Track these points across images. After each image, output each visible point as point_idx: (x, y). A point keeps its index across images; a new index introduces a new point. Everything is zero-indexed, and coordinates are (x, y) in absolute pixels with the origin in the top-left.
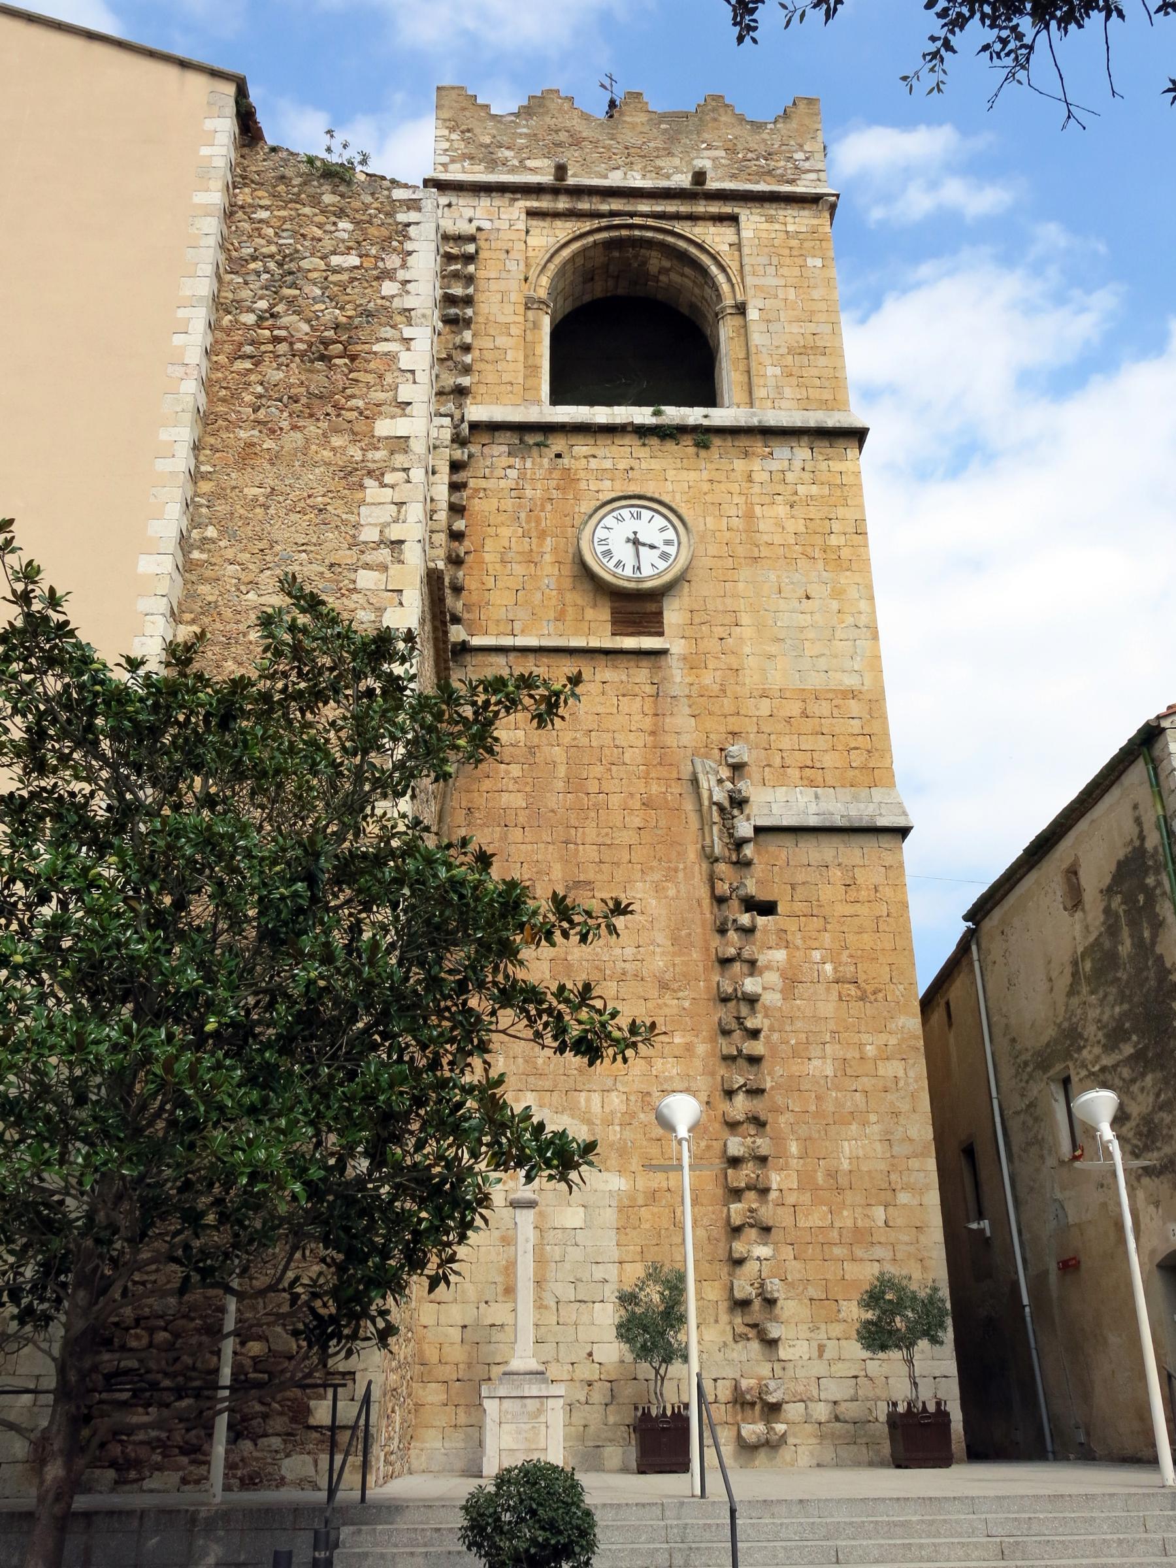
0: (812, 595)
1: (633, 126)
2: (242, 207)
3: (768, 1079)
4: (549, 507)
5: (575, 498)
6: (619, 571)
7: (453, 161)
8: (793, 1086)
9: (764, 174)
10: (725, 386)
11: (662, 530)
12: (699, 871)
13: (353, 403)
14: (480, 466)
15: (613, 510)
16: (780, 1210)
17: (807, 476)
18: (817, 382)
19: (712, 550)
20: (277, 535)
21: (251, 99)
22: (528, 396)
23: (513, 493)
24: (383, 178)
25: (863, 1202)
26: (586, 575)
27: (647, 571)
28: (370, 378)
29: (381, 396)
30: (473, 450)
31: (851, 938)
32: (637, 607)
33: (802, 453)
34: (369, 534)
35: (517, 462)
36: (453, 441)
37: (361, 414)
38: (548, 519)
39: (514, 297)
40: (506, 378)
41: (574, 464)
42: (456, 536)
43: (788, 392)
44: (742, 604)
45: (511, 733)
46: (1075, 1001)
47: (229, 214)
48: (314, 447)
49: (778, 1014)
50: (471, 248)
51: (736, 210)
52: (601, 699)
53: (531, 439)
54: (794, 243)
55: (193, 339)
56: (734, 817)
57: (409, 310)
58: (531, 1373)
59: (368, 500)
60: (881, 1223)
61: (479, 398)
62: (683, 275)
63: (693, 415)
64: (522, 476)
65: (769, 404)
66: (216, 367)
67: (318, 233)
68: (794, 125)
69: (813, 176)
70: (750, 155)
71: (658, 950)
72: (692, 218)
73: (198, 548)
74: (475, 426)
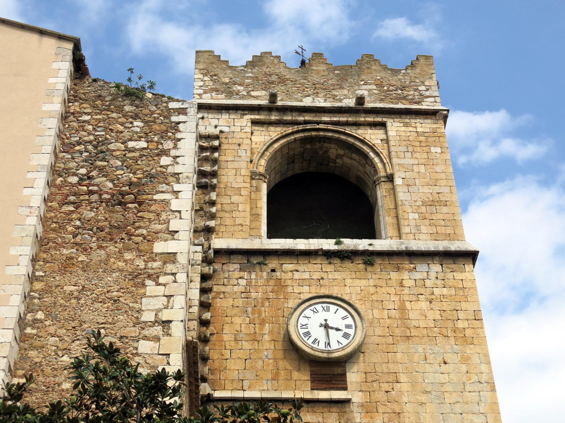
0: (448, 361)
1: (318, 72)
2: (73, 113)
4: (267, 304)
9: (401, 98)
10: (382, 223)
11: (344, 318)
14: (221, 277)
15: (311, 305)
17: (439, 282)
18: (443, 223)
19: (378, 331)
20: (85, 317)
21: (82, 52)
22: (253, 233)
24: (163, 96)
26: (292, 349)
27: (334, 346)
28: (151, 216)
29: (159, 227)
30: (216, 267)
32: (328, 370)
33: (436, 268)
34: (148, 317)
35: (246, 275)
36: (203, 261)
38: (266, 312)
39: (243, 172)
40: (238, 221)
41: (284, 276)
42: (204, 323)
43: (423, 229)
47: (64, 118)
48: (112, 260)
50: (216, 143)
51: (384, 120)
53: (254, 260)
54: (422, 138)
59: (148, 294)
61: (220, 234)
62: (351, 158)
63: (362, 244)
64: (249, 284)
65: (412, 236)
66: (50, 209)
67: (121, 128)
68: (418, 70)
69: (432, 99)
70: (391, 88)
72: (357, 125)
73: (31, 326)
74: (218, 252)
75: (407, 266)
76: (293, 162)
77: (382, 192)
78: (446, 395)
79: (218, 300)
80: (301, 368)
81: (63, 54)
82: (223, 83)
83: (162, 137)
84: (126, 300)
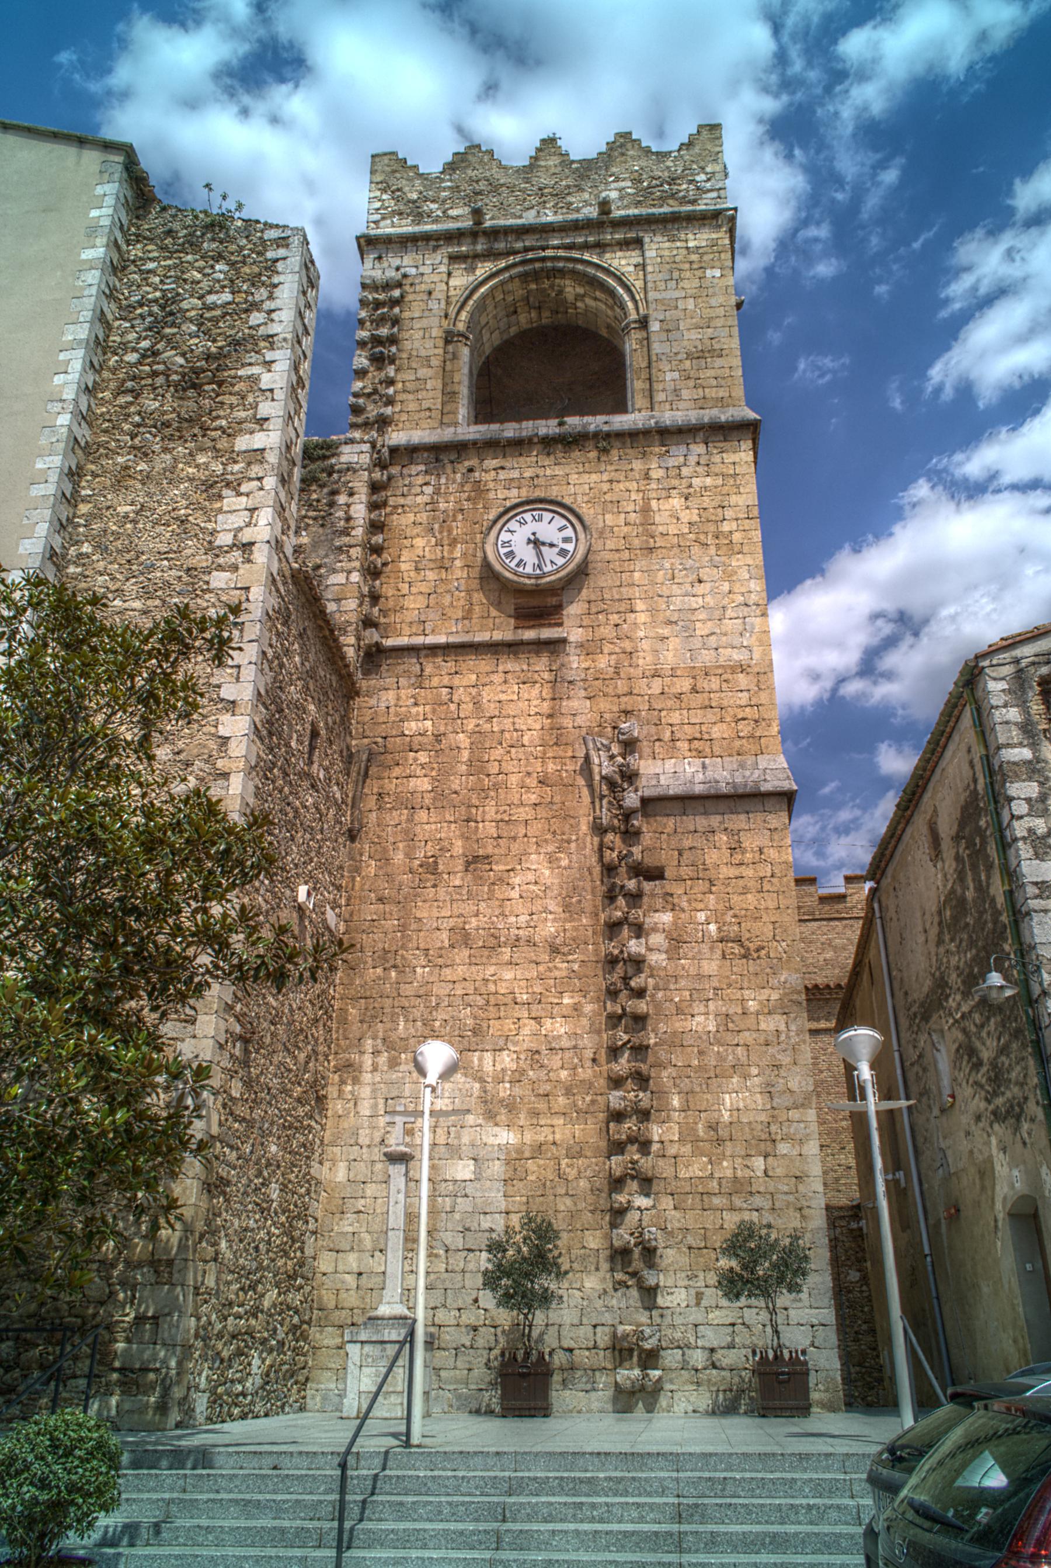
0: (705, 578)
2: (134, 261)
3: (652, 1035)
4: (460, 517)
5: (484, 507)
6: (521, 569)
7: (383, 219)
8: (676, 1041)
11: (561, 529)
12: (591, 842)
13: (217, 423)
16: (661, 1162)
18: (714, 383)
19: (610, 544)
23: (428, 508)
24: (258, 222)
25: (743, 1153)
28: (234, 400)
29: (243, 414)
31: (735, 899)
34: (224, 539)
35: (433, 480)
37: (224, 432)
38: (458, 528)
39: (436, 332)
40: (426, 404)
41: (485, 477)
43: (685, 394)
44: (637, 592)
45: (420, 724)
46: (942, 950)
48: (181, 466)
49: (662, 974)
50: (396, 293)
51: (641, 234)
52: (504, 688)
54: (694, 257)
55: (70, 375)
56: (624, 790)
57: (272, 336)
58: (395, 1318)
59: (225, 508)
60: (760, 1173)
62: (595, 299)
64: (437, 492)
65: (668, 406)
69: (714, 194)
71: (550, 917)
72: (600, 247)
74: (394, 450)
75: (657, 449)
76: (515, 312)
77: (631, 344)
78: (698, 625)
79: (395, 516)
80: (503, 601)
81: (111, 170)
82: (409, 201)
83: (253, 285)
84: (197, 519)
